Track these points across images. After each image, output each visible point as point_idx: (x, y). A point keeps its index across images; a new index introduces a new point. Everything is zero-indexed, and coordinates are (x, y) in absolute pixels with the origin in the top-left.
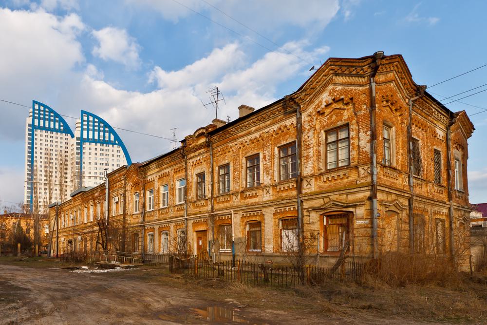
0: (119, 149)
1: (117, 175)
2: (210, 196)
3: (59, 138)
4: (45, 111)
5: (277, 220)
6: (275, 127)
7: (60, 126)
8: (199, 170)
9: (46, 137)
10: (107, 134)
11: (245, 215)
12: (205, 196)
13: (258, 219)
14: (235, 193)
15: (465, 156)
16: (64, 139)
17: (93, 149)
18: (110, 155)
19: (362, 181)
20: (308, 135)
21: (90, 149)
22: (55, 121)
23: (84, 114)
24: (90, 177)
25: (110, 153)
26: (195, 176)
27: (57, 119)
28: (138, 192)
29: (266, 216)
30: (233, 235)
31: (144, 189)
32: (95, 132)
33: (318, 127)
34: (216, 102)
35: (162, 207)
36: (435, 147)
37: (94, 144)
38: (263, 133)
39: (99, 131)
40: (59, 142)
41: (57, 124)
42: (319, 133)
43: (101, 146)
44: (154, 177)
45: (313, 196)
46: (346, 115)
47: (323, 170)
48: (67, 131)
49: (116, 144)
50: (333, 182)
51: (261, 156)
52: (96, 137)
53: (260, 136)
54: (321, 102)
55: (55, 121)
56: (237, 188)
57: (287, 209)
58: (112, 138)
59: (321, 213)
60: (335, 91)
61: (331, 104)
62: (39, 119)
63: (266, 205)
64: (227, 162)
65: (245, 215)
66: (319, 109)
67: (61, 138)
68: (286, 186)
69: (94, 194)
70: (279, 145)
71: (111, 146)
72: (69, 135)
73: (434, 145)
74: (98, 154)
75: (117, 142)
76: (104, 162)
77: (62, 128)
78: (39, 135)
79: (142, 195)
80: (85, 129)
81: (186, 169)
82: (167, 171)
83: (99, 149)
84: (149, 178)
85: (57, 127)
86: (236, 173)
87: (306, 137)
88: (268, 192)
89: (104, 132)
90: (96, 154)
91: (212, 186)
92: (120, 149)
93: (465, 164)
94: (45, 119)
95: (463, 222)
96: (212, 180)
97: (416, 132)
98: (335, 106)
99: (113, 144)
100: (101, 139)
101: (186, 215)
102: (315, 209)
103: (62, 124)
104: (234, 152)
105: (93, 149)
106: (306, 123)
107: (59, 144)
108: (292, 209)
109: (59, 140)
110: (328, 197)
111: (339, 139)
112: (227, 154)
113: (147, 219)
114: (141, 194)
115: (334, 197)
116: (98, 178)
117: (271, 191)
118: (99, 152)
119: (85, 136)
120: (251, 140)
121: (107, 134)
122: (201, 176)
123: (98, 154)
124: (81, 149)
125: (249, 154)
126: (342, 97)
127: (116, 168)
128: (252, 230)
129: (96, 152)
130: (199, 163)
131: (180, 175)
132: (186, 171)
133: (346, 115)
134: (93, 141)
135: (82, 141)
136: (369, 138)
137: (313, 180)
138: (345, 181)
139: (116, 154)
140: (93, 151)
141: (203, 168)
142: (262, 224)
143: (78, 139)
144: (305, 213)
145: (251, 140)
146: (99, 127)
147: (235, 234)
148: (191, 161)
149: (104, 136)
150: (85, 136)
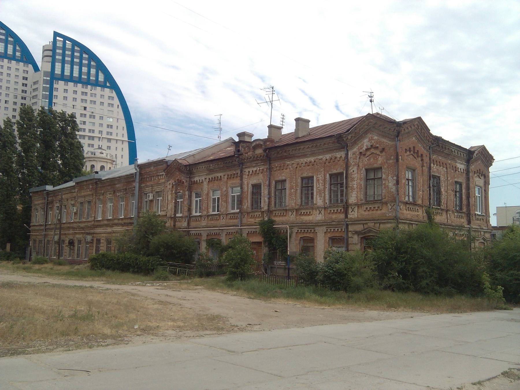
1: (152, 168)
2: (266, 208)
3: (13, 69)
5: (328, 238)
6: (328, 156)
7: (15, 50)
8: (254, 180)
9: (24, 79)
10: (93, 71)
11: (300, 231)
12: (261, 208)
13: (311, 235)
14: (292, 210)
15: (487, 183)
16: (21, 71)
17: (70, 91)
18: (98, 103)
19: (390, 214)
20: (353, 169)
21: (75, 92)
23: (58, 38)
25: (98, 100)
26: (250, 186)
28: (181, 191)
29: (318, 234)
30: (288, 249)
31: (190, 189)
33: (361, 165)
34: (271, 102)
36: (456, 180)
38: (317, 159)
39: (81, 65)
40: (13, 76)
42: (361, 170)
43: (83, 87)
44: (203, 179)
45: (356, 222)
46: (380, 160)
47: (363, 202)
48: (27, 57)
49: (107, 87)
50: (371, 212)
51: (315, 178)
53: (315, 161)
54: (363, 145)
56: (293, 204)
57: (336, 230)
58: (101, 78)
59: (362, 236)
60: (373, 139)
61: (370, 149)
63: (318, 224)
64: (284, 178)
65: (300, 231)
66: (361, 151)
67: (17, 69)
68: (336, 209)
69: (115, 184)
70: (330, 173)
71: (99, 88)
73: (455, 178)
75: (108, 84)
79: (187, 197)
82: (219, 175)
83: (79, 93)
84: (196, 179)
86: (292, 191)
87: (352, 171)
88: (320, 212)
89: (89, 67)
90: (75, 99)
91: (269, 198)
92: (114, 94)
93: (487, 190)
95: (483, 241)
96: (269, 193)
97: (437, 170)
98: (372, 150)
99: (103, 86)
100: (83, 77)
101: (240, 226)
102: (356, 233)
103: (18, 48)
104: (290, 173)
105: (70, 91)
106: (352, 159)
107: (13, 79)
108: (340, 230)
109: (13, 72)
110: (367, 223)
111: (376, 177)
112: (284, 170)
113: (193, 224)
114: (185, 195)
115: (371, 225)
116: (87, 138)
117: (323, 212)
118: (79, 96)
120: (306, 163)
121: (93, 71)
122: (257, 187)
125: (305, 175)
126: (378, 145)
128: (305, 245)
129: (75, 96)
130: (255, 173)
131: (234, 182)
132: (241, 179)
133: (380, 160)
134: (71, 79)
136: (395, 182)
137: (356, 208)
138: (379, 212)
139: (106, 101)
140: (70, 95)
142: (315, 241)
144: (350, 235)
145: (306, 163)
147: (290, 247)
148: (247, 170)
150: (58, 71)
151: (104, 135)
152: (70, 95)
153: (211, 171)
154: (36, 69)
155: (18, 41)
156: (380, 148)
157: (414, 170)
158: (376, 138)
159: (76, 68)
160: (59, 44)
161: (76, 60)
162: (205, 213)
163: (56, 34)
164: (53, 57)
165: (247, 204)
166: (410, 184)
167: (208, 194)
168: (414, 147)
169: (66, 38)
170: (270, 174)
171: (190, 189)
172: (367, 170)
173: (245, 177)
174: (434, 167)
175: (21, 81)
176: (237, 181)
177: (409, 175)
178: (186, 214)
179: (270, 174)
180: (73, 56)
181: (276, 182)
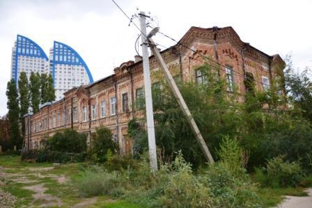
4: (26, 42)
7: (37, 52)
8: (123, 92)
10: (73, 58)
17: (63, 69)
21: (65, 69)
24: (60, 90)
33: (191, 67)
35: (101, 117)
39: (67, 55)
48: (43, 55)
52: (65, 60)
55: (34, 49)
58: (77, 60)
62: (22, 47)
71: (76, 66)
76: (72, 78)
81: (116, 90)
82: (104, 91)
84: (92, 96)
85: (35, 53)
89: (71, 55)
92: (84, 68)
99: (78, 64)
118: (67, 71)
121: (73, 58)
124: (54, 69)
127: (71, 88)
130: (123, 86)
132: (116, 92)
135: (53, 63)
139: (80, 71)
140: (63, 70)
141: (127, 90)
143: (51, 61)
146: (67, 52)
148: (119, 85)
150: (57, 59)
152: (63, 70)
153: (100, 90)
154: (47, 60)
155: (39, 48)
156: (204, 51)
157: (232, 67)
158: (199, 44)
159: (65, 57)
160: (57, 47)
161: (65, 53)
162: (98, 118)
163: (55, 42)
164: (54, 53)
165: (120, 109)
166: (230, 78)
167: (99, 106)
168: (229, 50)
169: (59, 43)
170: (132, 85)
171: (89, 104)
172: (196, 70)
173: (118, 90)
174: (247, 67)
175: (41, 66)
176: (113, 94)
177: (228, 71)
178: (88, 120)
179: (132, 85)
180: (63, 52)
181: (137, 90)
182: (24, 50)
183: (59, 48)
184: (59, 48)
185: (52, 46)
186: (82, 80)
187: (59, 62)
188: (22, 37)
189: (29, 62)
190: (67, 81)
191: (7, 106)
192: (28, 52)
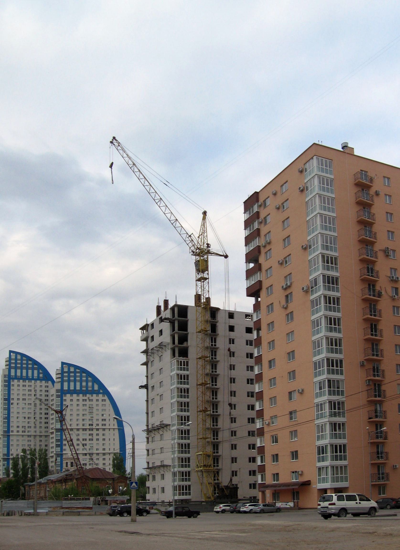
0: (104, 398)
4: (22, 360)
7: (39, 373)
10: (90, 384)
22: (33, 369)
27: (35, 366)
32: (71, 383)
37: (69, 395)
41: (36, 372)
43: (83, 396)
48: (47, 377)
49: (101, 393)
52: (78, 388)
55: (33, 369)
58: (96, 387)
62: (16, 368)
71: (95, 395)
72: (50, 382)
74: (81, 405)
75: (101, 391)
77: (41, 375)
78: (16, 385)
80: (13, 359)
92: (106, 398)
94: (22, 368)
99: (97, 393)
103: (41, 371)
109: (38, 389)
116: (88, 430)
118: (81, 403)
119: (66, 388)
123: (81, 405)
134: (75, 392)
149: (87, 386)
150: (66, 388)
151: (100, 426)
154: (53, 382)
155: (40, 367)
159: (78, 384)
160: (66, 370)
161: (78, 379)
180: (75, 376)
182: (19, 371)
183: (69, 372)
184: (69, 372)
185: (59, 366)
186: (103, 415)
187: (69, 392)
188: (17, 353)
189: (27, 388)
190: (81, 417)
191: (140, 474)
192: (19, 374)
